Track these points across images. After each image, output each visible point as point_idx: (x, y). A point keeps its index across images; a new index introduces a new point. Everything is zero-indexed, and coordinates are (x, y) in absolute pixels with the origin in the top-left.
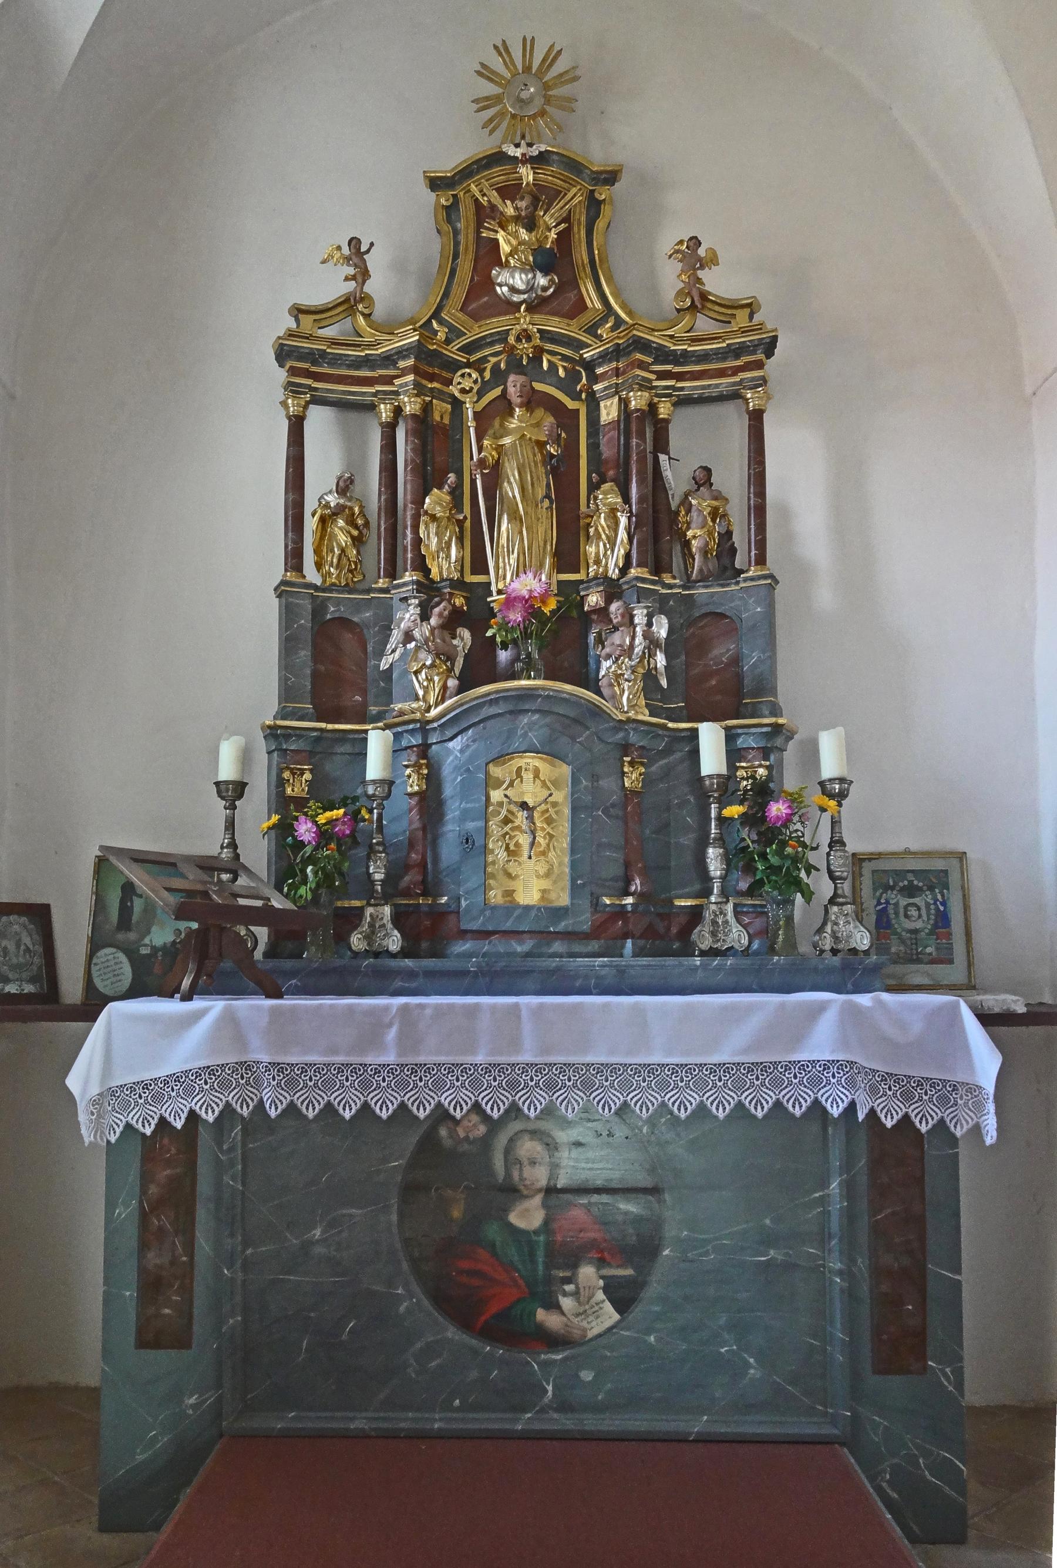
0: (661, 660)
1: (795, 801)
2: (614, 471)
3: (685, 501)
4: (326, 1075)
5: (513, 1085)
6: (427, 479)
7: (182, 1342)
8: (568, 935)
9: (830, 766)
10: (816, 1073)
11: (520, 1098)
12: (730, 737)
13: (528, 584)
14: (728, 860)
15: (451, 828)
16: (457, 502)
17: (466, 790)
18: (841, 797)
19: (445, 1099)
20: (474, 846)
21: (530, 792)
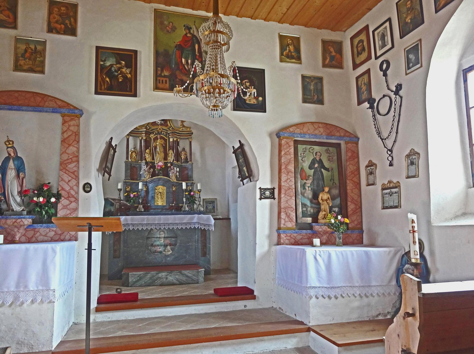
0: (178, 174)
1: (194, 192)
2: (171, 148)
3: (181, 152)
4: (138, 225)
5: (160, 226)
6: (147, 147)
7: (119, 257)
8: (165, 209)
9: (199, 188)
10: (194, 223)
11: (161, 227)
12: (187, 184)
13: (161, 164)
14: (186, 199)
15: (150, 195)
16: (150, 152)
17: (152, 190)
18: (200, 192)
19: (152, 227)
20: (153, 198)
21: (161, 191)
